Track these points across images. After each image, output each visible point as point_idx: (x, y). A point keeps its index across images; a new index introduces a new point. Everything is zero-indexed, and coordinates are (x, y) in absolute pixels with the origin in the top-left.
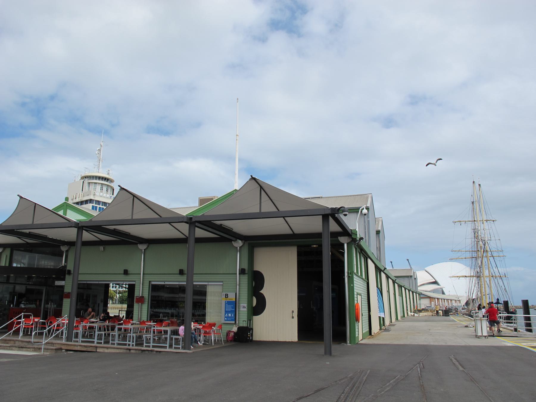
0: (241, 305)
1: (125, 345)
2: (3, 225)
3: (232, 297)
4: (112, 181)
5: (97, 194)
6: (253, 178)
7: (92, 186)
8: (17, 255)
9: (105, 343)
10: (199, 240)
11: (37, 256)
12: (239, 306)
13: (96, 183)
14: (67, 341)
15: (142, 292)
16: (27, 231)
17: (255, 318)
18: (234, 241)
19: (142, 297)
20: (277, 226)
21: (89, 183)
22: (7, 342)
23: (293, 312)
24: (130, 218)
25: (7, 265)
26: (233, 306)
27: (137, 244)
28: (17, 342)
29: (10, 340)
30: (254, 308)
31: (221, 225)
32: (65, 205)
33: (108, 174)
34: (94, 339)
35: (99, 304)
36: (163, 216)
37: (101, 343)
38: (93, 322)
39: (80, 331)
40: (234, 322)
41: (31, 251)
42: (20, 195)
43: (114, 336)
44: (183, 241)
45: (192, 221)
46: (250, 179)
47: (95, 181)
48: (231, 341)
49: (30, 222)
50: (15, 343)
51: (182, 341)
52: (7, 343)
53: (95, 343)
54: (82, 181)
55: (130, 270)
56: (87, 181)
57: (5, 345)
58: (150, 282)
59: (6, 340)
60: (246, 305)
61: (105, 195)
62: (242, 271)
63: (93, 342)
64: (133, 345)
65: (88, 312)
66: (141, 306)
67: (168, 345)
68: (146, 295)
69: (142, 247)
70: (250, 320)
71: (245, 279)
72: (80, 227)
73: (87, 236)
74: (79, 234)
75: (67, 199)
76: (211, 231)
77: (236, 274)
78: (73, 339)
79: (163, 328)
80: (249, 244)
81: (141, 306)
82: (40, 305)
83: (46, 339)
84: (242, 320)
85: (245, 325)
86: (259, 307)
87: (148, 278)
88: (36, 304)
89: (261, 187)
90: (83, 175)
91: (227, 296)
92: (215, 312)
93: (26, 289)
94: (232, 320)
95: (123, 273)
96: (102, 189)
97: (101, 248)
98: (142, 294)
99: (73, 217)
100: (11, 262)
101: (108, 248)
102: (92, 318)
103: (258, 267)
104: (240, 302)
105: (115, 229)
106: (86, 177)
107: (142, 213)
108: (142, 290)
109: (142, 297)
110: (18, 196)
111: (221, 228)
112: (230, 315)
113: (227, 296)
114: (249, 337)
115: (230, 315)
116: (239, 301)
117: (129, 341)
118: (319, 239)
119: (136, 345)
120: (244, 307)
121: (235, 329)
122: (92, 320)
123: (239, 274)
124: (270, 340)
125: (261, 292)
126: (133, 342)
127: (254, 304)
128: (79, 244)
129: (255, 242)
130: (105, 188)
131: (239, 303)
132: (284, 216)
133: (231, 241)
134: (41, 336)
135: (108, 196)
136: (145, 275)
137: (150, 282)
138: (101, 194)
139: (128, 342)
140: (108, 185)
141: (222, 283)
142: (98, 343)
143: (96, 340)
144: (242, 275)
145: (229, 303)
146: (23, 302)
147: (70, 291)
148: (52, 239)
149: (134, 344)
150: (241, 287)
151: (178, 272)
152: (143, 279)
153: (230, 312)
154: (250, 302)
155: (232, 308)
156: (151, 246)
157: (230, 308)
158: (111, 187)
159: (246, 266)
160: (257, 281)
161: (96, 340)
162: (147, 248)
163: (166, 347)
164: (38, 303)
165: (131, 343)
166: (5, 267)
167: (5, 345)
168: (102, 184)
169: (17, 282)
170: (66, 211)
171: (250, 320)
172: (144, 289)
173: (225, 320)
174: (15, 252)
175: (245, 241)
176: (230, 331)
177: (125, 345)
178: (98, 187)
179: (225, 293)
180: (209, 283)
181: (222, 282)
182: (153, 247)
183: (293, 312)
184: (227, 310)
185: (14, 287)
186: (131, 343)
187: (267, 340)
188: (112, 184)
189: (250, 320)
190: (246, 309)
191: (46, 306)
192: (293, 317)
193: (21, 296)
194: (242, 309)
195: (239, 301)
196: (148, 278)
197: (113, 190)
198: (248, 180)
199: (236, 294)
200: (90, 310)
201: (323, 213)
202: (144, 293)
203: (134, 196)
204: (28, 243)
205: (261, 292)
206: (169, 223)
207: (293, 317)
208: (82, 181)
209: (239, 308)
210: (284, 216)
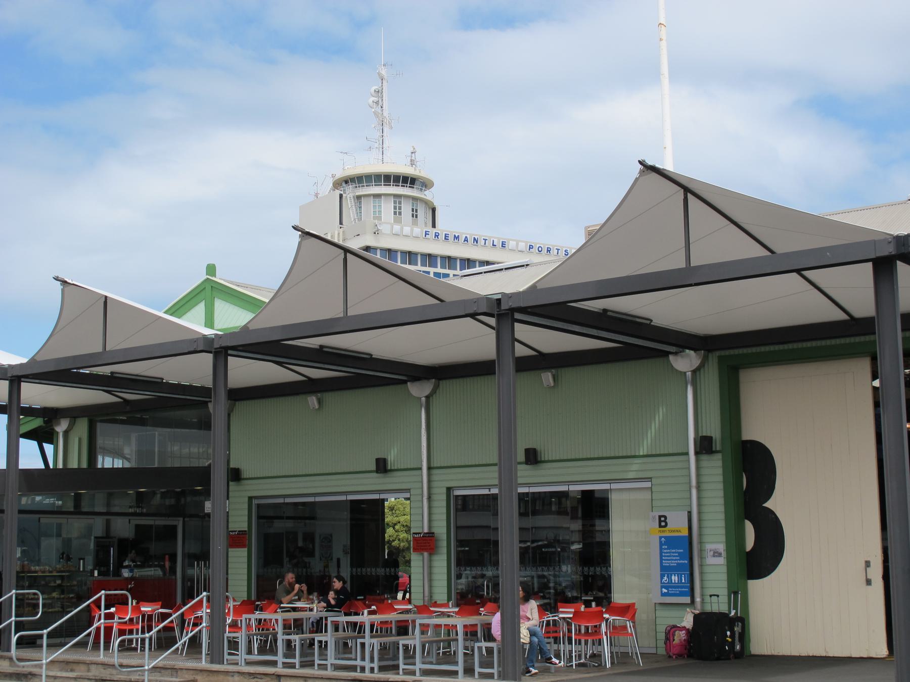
0: (708, 546)
1: (353, 668)
2: (251, 327)
3: (678, 525)
4: (426, 184)
5: (384, 228)
6: (649, 169)
7: (368, 206)
8: (107, 434)
9: (303, 665)
10: (240, 395)
11: (158, 433)
12: (701, 551)
13: (378, 196)
14: (212, 662)
15: (430, 521)
16: (106, 370)
17: (755, 586)
18: (676, 353)
19: (431, 535)
20: (782, 302)
21: (359, 198)
22: (74, 666)
23: (868, 564)
24: (683, 265)
25: (84, 465)
26: (683, 551)
27: (405, 382)
28: (93, 667)
29: (78, 663)
30: (750, 556)
31: (605, 311)
32: (208, 288)
33: (413, 163)
34: (276, 654)
35: (338, 560)
36: (779, 249)
37: (292, 666)
38: (732, 636)
39: (241, 637)
40: (687, 600)
41: (142, 422)
42: (61, 276)
43: (323, 646)
44: (480, 369)
45: (550, 308)
46: (641, 173)
47: (393, 190)
48: (680, 656)
49: (679, 263)
50: (89, 671)
51: (499, 652)
52: (72, 670)
53: (280, 665)
54: (338, 192)
55: (393, 458)
56: (350, 192)
57: (64, 674)
58: (449, 490)
59: (164, 668)
60: (721, 547)
61: (407, 230)
62: (705, 446)
63: (274, 663)
64: (372, 670)
65: (286, 583)
66: (430, 561)
67: (460, 668)
68: (440, 529)
69: (419, 390)
70: (737, 592)
71: (715, 466)
72: (222, 350)
73: (246, 371)
74: (505, 338)
75: (211, 269)
76: (586, 333)
77: (687, 454)
78: (226, 656)
79: (392, 617)
80: (721, 359)
81: (430, 561)
82: (173, 570)
83: (152, 658)
84: (714, 595)
85: (720, 605)
86: (762, 555)
87: (444, 480)
88: (163, 567)
89: (687, 190)
90: (340, 174)
91: (663, 521)
92: (634, 571)
93: (138, 527)
94: (682, 594)
95: (374, 468)
96: (397, 212)
97: (313, 400)
98: (430, 527)
99: (194, 323)
100: (92, 459)
101: (570, 375)
102: (299, 600)
103: (751, 432)
104: (706, 539)
105: (321, 347)
106: (348, 181)
107: (718, 245)
108: (430, 514)
109: (431, 535)
110: (57, 279)
111: (322, 356)
112: (675, 578)
113: (663, 521)
114: (732, 645)
115: (675, 578)
116: (700, 535)
117: (363, 659)
118: (867, 338)
119: (382, 669)
120: (717, 554)
121: (688, 621)
122: (299, 605)
123: (697, 453)
124: (804, 654)
125: (767, 505)
126: (372, 660)
127: (750, 543)
128: (222, 395)
129: (737, 354)
130: (406, 208)
131: (701, 543)
132: (800, 266)
133: (666, 354)
134: (198, 656)
135: (417, 231)
136: (434, 472)
137: (449, 490)
138: (397, 228)
139: (359, 662)
140: (415, 199)
141: (648, 484)
142: (286, 665)
143: (280, 658)
144: (704, 457)
145: (669, 542)
146: (126, 563)
147: (244, 526)
148: (191, 386)
149: (375, 665)
150: (702, 497)
151: (373, 467)
152: (429, 481)
153: (676, 569)
154: (735, 537)
155: (681, 556)
156: (443, 383)
157: (675, 558)
158: (426, 203)
159: (713, 429)
160: (752, 472)
161: (280, 658)
162: (434, 392)
163: (455, 673)
164: (167, 564)
165: (367, 664)
166: (79, 470)
167: (64, 674)
168: (395, 196)
169: (116, 509)
170: (213, 305)
171: (737, 592)
172: (435, 510)
173: (663, 595)
174: (100, 427)
175: (709, 351)
176: (675, 627)
177: (353, 668)
178: (387, 207)
179: (657, 514)
180: (614, 486)
181: (649, 479)
182: (452, 388)
183: (868, 564)
184: (666, 563)
185: (108, 523)
186: (367, 664)
187: (795, 653)
188: (428, 195)
189: (736, 593)
190: (722, 561)
191: (190, 572)
192: (869, 582)
193: (124, 547)
194: (710, 560)
195: (700, 535)
196: (444, 480)
197: (434, 210)
198: (297, 240)
199: (690, 513)
200: (290, 577)
201: (873, 256)
202: (435, 524)
203: (687, 190)
204: (310, 379)
205: (767, 505)
206: (799, 271)
207: (869, 582)
208: (338, 192)
209: (701, 558)
210: (800, 266)
